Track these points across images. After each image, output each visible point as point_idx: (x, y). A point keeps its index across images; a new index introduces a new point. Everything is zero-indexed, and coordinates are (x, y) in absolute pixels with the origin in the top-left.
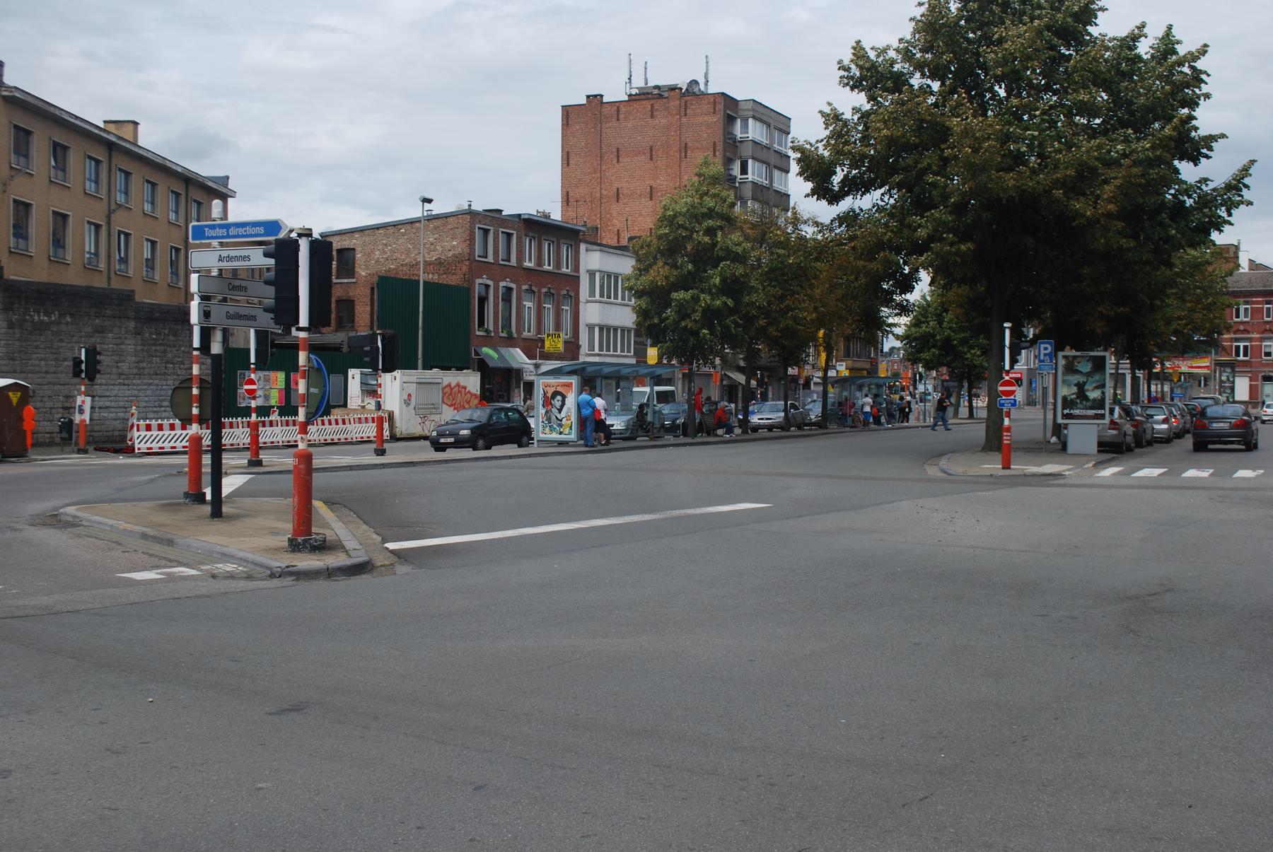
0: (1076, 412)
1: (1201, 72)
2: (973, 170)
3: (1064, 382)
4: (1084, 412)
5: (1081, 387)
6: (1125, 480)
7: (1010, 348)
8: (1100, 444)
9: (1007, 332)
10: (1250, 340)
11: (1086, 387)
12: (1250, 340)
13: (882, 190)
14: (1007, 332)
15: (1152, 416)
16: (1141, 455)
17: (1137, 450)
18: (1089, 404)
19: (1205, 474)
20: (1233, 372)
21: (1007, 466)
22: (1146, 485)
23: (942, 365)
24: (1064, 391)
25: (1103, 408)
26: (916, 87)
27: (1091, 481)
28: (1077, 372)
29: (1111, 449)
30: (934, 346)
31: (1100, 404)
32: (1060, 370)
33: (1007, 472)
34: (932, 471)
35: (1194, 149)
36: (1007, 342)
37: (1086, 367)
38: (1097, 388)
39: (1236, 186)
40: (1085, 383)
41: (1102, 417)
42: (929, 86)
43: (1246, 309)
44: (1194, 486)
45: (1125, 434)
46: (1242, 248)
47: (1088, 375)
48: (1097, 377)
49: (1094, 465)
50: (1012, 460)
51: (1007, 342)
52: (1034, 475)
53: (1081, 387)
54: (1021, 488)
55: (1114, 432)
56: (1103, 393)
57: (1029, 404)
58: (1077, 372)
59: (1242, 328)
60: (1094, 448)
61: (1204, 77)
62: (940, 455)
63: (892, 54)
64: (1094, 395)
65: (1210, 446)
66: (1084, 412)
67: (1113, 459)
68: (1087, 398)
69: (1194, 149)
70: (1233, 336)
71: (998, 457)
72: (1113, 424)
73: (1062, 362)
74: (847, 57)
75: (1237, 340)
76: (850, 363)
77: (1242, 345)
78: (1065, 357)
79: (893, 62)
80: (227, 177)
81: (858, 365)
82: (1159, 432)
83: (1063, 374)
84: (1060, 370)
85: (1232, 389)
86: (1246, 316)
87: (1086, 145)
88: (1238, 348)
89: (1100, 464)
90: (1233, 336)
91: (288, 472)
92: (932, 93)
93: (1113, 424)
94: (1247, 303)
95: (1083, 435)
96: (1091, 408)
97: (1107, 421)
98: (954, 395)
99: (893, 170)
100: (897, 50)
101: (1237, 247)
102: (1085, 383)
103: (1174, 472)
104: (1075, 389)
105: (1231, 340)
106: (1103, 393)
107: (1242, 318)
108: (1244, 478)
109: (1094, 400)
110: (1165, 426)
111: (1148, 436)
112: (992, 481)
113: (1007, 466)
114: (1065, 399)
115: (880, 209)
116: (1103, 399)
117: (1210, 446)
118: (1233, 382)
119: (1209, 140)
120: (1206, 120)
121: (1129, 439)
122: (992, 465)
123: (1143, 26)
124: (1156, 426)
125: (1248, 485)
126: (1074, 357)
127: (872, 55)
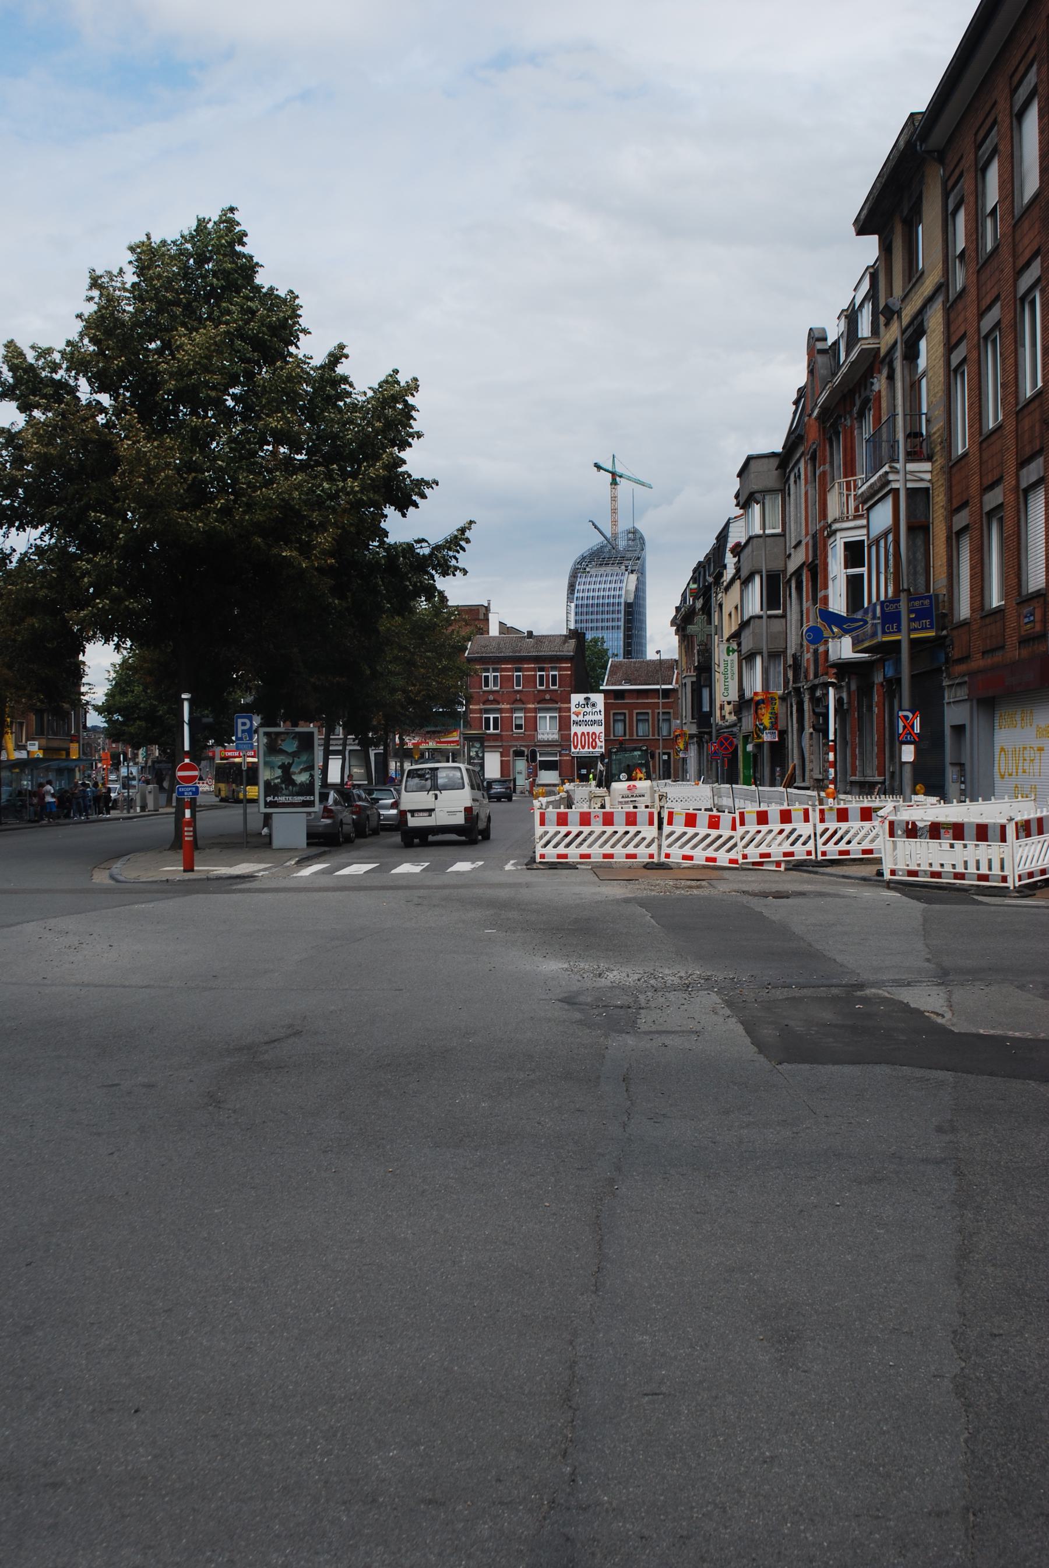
0: (282, 799)
1: (413, 408)
2: (150, 507)
4: (290, 799)
5: (286, 769)
6: (325, 881)
7: (190, 724)
8: (310, 836)
9: (186, 705)
10: (500, 711)
12: (500, 711)
13: (41, 529)
14: (186, 705)
15: (377, 800)
16: (359, 847)
17: (358, 841)
19: (416, 869)
20: (482, 746)
21: (189, 868)
22: (355, 885)
23: (152, 742)
25: (313, 794)
26: (84, 402)
27: (291, 884)
28: (282, 752)
29: (325, 841)
30: (139, 718)
31: (307, 789)
33: (189, 875)
34: (101, 878)
35: (405, 494)
36: (186, 718)
37: (291, 746)
39: (457, 541)
40: (290, 765)
41: (311, 804)
42: (99, 403)
43: (495, 677)
44: (407, 884)
45: (341, 823)
46: (492, 609)
47: (294, 754)
48: (304, 758)
49: (298, 863)
50: (195, 858)
51: (186, 718)
52: (219, 878)
54: (195, 896)
55: (328, 821)
56: (312, 776)
58: (282, 752)
59: (491, 697)
60: (302, 841)
61: (413, 413)
62: (118, 855)
63: (57, 357)
64: (302, 778)
65: (431, 838)
66: (290, 799)
67: (330, 852)
68: (293, 783)
69: (405, 494)
70: (482, 707)
71: (180, 856)
72: (327, 812)
74: (403, 379)
75: (487, 711)
76: (44, 742)
77: (491, 716)
79: (55, 367)
81: (55, 744)
82: (388, 818)
85: (482, 766)
86: (495, 685)
87: (283, 483)
88: (488, 719)
89: (304, 861)
90: (482, 707)
91: (555, 660)
92: (103, 410)
93: (327, 812)
94: (495, 670)
95: (291, 827)
96: (298, 794)
97: (318, 808)
98: (168, 778)
99: (49, 500)
100: (63, 353)
101: (487, 609)
102: (290, 765)
103: (384, 868)
104: (279, 772)
105: (481, 711)
106: (312, 776)
107: (492, 687)
108: (457, 873)
109: (302, 784)
110: (394, 812)
111: (373, 823)
112: (169, 888)
113: (189, 868)
115: (39, 551)
116: (312, 783)
118: (483, 758)
119: (420, 486)
120: (416, 461)
121: (348, 829)
122: (173, 869)
123: (341, 347)
124: (382, 812)
125: (464, 881)
127: (30, 356)
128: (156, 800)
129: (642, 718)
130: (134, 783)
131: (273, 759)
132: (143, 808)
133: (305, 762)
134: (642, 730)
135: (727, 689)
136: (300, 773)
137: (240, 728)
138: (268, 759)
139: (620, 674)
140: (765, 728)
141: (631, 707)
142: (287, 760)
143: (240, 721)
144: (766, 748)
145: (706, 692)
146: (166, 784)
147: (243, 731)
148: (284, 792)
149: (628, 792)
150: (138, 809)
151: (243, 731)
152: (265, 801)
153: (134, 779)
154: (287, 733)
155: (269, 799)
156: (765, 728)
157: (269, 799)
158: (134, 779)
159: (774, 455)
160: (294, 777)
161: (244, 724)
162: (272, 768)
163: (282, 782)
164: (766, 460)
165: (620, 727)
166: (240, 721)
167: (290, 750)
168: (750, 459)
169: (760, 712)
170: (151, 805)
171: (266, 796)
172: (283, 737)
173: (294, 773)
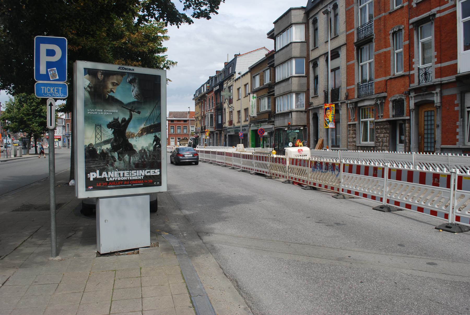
0: (113, 175)
3: (88, 119)
5: (119, 128)
11: (130, 129)
18: (135, 159)
24: (88, 136)
32: (81, 95)
37: (126, 93)
38: (147, 131)
40: (126, 123)
47: (132, 107)
48: (146, 112)
53: (119, 128)
56: (157, 140)
57: (63, 147)
64: (141, 143)
65: (220, 122)
66: (127, 175)
68: (130, 149)
73: (82, 82)
78: (88, 71)
80: (85, 69)
83: (86, 104)
84: (81, 95)
91: (279, 65)
96: (138, 166)
104: (109, 134)
106: (157, 140)
109: (143, 152)
114: (91, 153)
117: (220, 122)
126: (108, 74)
128: (21, 153)
129: (179, 128)
130: (9, 146)
131: (99, 111)
132: (15, 155)
133: (148, 119)
134: (179, 131)
135: (253, 112)
136: (141, 135)
137: (44, 59)
138: (91, 112)
139: (172, 115)
140: (330, 121)
141: (176, 124)
142: (122, 116)
143: (44, 47)
144: (330, 130)
145: (220, 117)
146: (27, 146)
147: (49, 65)
148: (116, 164)
149: (298, 153)
150: (13, 156)
151: (49, 65)
152: (87, 179)
153: (10, 144)
154: (122, 74)
155: (92, 176)
156: (330, 121)
157: (92, 176)
158: (10, 144)
159: (303, 8)
160: (132, 141)
161: (51, 53)
162: (98, 126)
163: (114, 149)
164: (298, 11)
165: (172, 130)
166: (44, 47)
167: (126, 101)
168: (290, 10)
169: (327, 113)
170: (18, 154)
171: (87, 172)
172: (114, 79)
173: (132, 136)
